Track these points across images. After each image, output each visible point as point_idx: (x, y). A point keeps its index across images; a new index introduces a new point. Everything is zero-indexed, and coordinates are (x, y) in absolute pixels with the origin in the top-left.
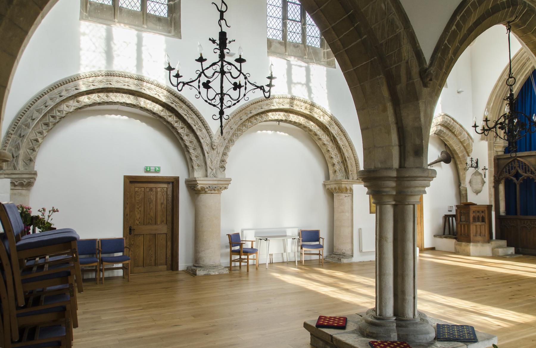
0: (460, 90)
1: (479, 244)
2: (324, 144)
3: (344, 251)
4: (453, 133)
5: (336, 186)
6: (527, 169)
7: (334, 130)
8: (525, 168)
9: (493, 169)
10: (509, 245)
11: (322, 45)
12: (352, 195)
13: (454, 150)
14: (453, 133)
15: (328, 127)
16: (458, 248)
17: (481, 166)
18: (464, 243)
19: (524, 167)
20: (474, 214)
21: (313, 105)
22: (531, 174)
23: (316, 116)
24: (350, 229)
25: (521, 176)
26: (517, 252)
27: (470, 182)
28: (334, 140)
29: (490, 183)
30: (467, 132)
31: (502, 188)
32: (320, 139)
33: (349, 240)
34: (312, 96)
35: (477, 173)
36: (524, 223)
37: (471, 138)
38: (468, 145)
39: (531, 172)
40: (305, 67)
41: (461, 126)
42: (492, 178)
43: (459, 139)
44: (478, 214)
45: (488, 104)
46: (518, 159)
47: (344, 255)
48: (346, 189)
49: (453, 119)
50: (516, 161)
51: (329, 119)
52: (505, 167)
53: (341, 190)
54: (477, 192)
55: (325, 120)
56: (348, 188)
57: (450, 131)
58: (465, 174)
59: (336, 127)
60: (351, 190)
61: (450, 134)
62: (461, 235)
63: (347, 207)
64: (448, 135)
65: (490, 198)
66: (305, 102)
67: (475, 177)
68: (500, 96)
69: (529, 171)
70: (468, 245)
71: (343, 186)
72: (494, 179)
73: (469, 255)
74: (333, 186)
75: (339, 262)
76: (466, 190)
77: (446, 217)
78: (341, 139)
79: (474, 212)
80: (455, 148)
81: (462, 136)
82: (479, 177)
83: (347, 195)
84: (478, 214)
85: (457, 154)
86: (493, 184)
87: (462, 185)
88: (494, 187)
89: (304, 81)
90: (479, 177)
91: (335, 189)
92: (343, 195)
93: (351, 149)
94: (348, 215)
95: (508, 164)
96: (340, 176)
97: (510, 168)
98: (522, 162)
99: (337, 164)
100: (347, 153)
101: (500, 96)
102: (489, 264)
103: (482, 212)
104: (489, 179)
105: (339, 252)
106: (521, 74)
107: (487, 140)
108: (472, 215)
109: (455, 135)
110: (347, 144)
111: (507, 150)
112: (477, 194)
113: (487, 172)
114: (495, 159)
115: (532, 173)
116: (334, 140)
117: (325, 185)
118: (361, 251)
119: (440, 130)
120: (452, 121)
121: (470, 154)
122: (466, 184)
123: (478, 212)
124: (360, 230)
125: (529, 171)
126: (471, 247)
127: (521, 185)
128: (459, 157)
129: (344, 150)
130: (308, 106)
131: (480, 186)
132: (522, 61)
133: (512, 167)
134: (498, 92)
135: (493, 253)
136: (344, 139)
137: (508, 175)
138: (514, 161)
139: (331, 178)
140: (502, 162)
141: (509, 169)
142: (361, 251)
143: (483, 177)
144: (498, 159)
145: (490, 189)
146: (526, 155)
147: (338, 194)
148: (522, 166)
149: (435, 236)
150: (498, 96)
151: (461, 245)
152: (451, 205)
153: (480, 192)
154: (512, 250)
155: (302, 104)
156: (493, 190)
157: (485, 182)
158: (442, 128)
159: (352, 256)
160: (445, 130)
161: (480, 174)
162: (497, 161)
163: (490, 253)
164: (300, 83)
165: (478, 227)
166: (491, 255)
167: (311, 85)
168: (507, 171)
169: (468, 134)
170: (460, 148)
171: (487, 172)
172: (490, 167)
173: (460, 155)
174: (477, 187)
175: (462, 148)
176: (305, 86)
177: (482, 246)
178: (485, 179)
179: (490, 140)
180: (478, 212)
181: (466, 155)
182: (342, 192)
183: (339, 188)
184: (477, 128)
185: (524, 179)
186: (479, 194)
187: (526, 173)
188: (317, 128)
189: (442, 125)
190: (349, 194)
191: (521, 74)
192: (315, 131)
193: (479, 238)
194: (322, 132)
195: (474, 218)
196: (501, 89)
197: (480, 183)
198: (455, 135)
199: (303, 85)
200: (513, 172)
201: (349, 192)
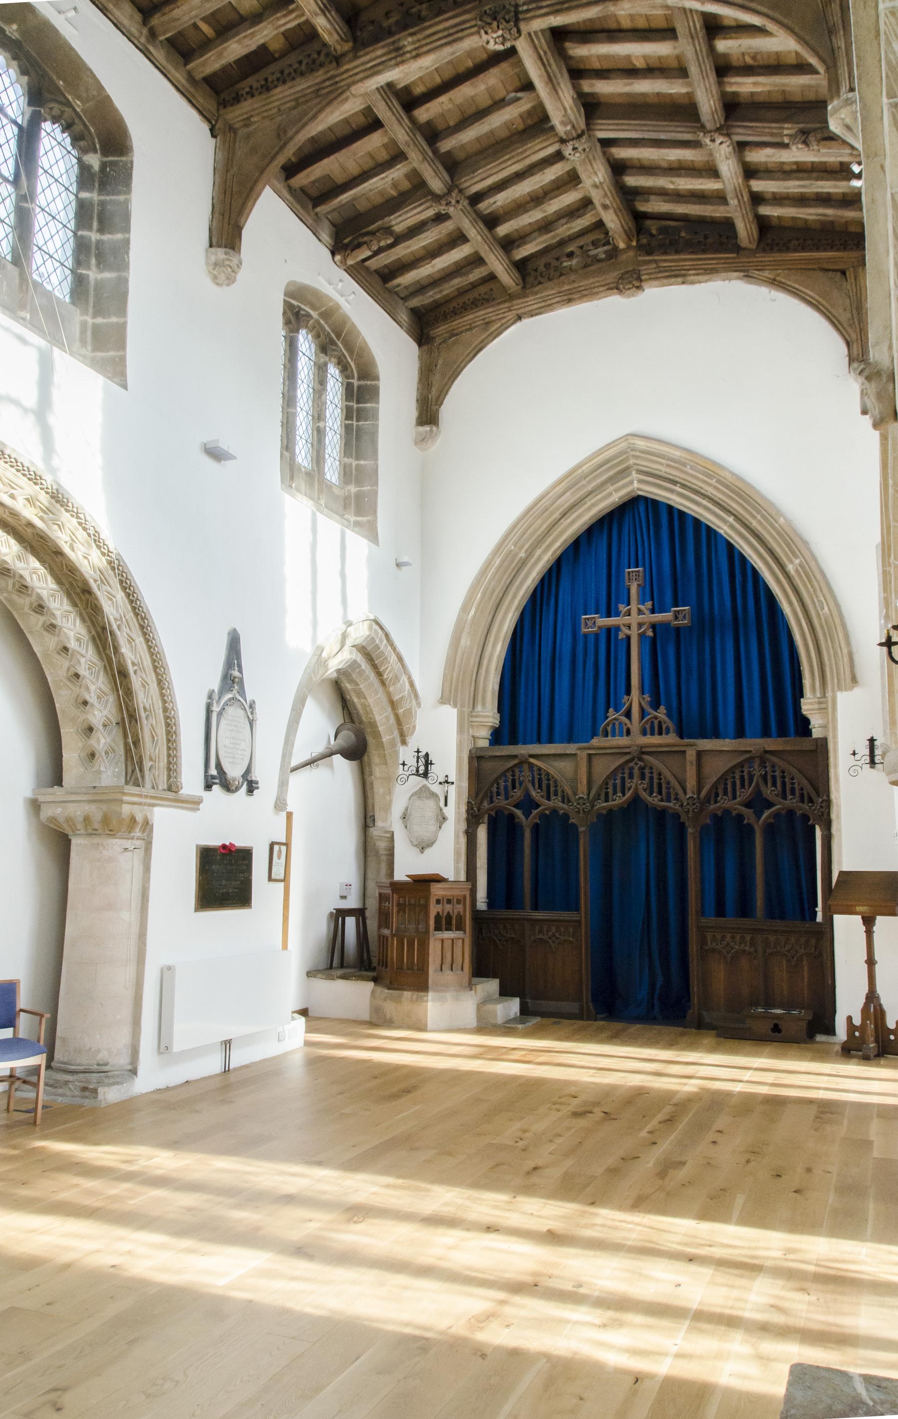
0: (405, 559)
1: (449, 995)
2: (66, 649)
3: (102, 1056)
4: (379, 674)
5: (96, 812)
6: (552, 789)
7: (113, 606)
8: (548, 786)
9: (465, 784)
10: (505, 992)
11: (226, 253)
12: (148, 844)
13: (373, 725)
14: (379, 674)
15: (94, 586)
16: (390, 1008)
17: (437, 771)
18: (407, 994)
19: (545, 782)
20: (439, 908)
21: (58, 498)
22: (563, 802)
23: (62, 539)
24: (131, 969)
25: (537, 806)
26: (525, 1011)
27: (404, 817)
28: (102, 637)
29: (457, 821)
30: (410, 678)
31: (482, 834)
32: (52, 627)
33: (126, 1013)
34: (56, 462)
35: (424, 793)
36: (541, 931)
37: (416, 696)
38: (409, 713)
39: (563, 797)
40: (40, 350)
41: (400, 659)
42: (464, 808)
43: (389, 695)
44: (448, 908)
45: (465, 609)
46: (532, 760)
47: (102, 1073)
48: (133, 820)
49: (387, 635)
50: (526, 767)
51: (102, 563)
52: (496, 781)
53: (111, 825)
54: (423, 846)
55: (87, 560)
56: (139, 818)
57: (375, 667)
58: (389, 792)
59: (120, 595)
60: (147, 826)
61: (372, 676)
62: (400, 968)
63: (128, 889)
64: (368, 678)
65: (457, 861)
66: (36, 479)
67: (418, 803)
68: (492, 594)
69: (556, 794)
70: (420, 1000)
71: (126, 809)
72: (467, 811)
73: (422, 1028)
74: (77, 811)
75: (87, 1103)
76: (392, 839)
77: (340, 915)
78: (130, 640)
79: (438, 902)
80: (378, 718)
81: (398, 685)
82: (430, 805)
83: (128, 844)
84: (448, 908)
85: (377, 735)
86: (463, 826)
87: (379, 823)
88: (466, 832)
89: (31, 399)
90: (431, 803)
91: (87, 820)
92: (116, 845)
93: (159, 682)
94: (128, 917)
95: (504, 774)
96: (110, 773)
97: (510, 784)
98: (540, 769)
99: (101, 728)
100: (145, 695)
101: (492, 594)
102: (516, 1055)
103: (458, 902)
104: (455, 811)
105: (84, 1061)
106: (544, 546)
107: (455, 706)
108: (434, 910)
109: (383, 683)
110: (147, 662)
111: (497, 737)
112: (422, 849)
113: (452, 790)
114: (471, 758)
115: (565, 799)
116: (102, 637)
117: (35, 806)
118: (163, 1048)
119: (355, 662)
120: (385, 642)
121: (408, 739)
122: (391, 820)
123: (449, 901)
124: (166, 972)
125: (556, 794)
126: (430, 1004)
127: (536, 828)
128: (380, 745)
129: (136, 682)
130: (44, 498)
131: (433, 828)
132: (552, 513)
133: (513, 781)
134: (489, 583)
135: (479, 1018)
136: (140, 640)
137: (501, 802)
138: (521, 763)
139: (68, 777)
140: (487, 766)
141: (506, 787)
142: (163, 1048)
143: (442, 803)
144: (479, 758)
145: (457, 837)
146: (552, 752)
147: (96, 840)
148: (540, 780)
149: (310, 974)
150: (488, 592)
151: (398, 1000)
152: (349, 882)
153: (430, 845)
154: (513, 1006)
155: (23, 481)
156: (463, 840)
157: (444, 819)
158: (360, 658)
159: (134, 1072)
160: (364, 665)
161: (434, 795)
162: (477, 762)
163: (471, 1019)
164: (16, 403)
165: (448, 944)
166: (473, 1022)
167: (52, 420)
168: (503, 792)
169: (412, 684)
170: (387, 718)
171: (452, 790)
172: (459, 779)
173: (385, 739)
174: (424, 830)
175: (392, 720)
176: (31, 418)
177: (457, 999)
178: (446, 810)
179: (462, 706)
180: (449, 901)
181: (398, 740)
182: (112, 833)
183: (106, 820)
184: (893, 648)
185: (542, 816)
186: (427, 851)
187: (549, 799)
188: (52, 584)
189: (362, 649)
190: (138, 843)
191: (544, 546)
192: (44, 593)
193: (448, 976)
194: (66, 606)
195: (438, 917)
196: (496, 578)
197: (433, 822)
198: (383, 683)
199: (26, 410)
200: (518, 794)
201: (137, 833)
